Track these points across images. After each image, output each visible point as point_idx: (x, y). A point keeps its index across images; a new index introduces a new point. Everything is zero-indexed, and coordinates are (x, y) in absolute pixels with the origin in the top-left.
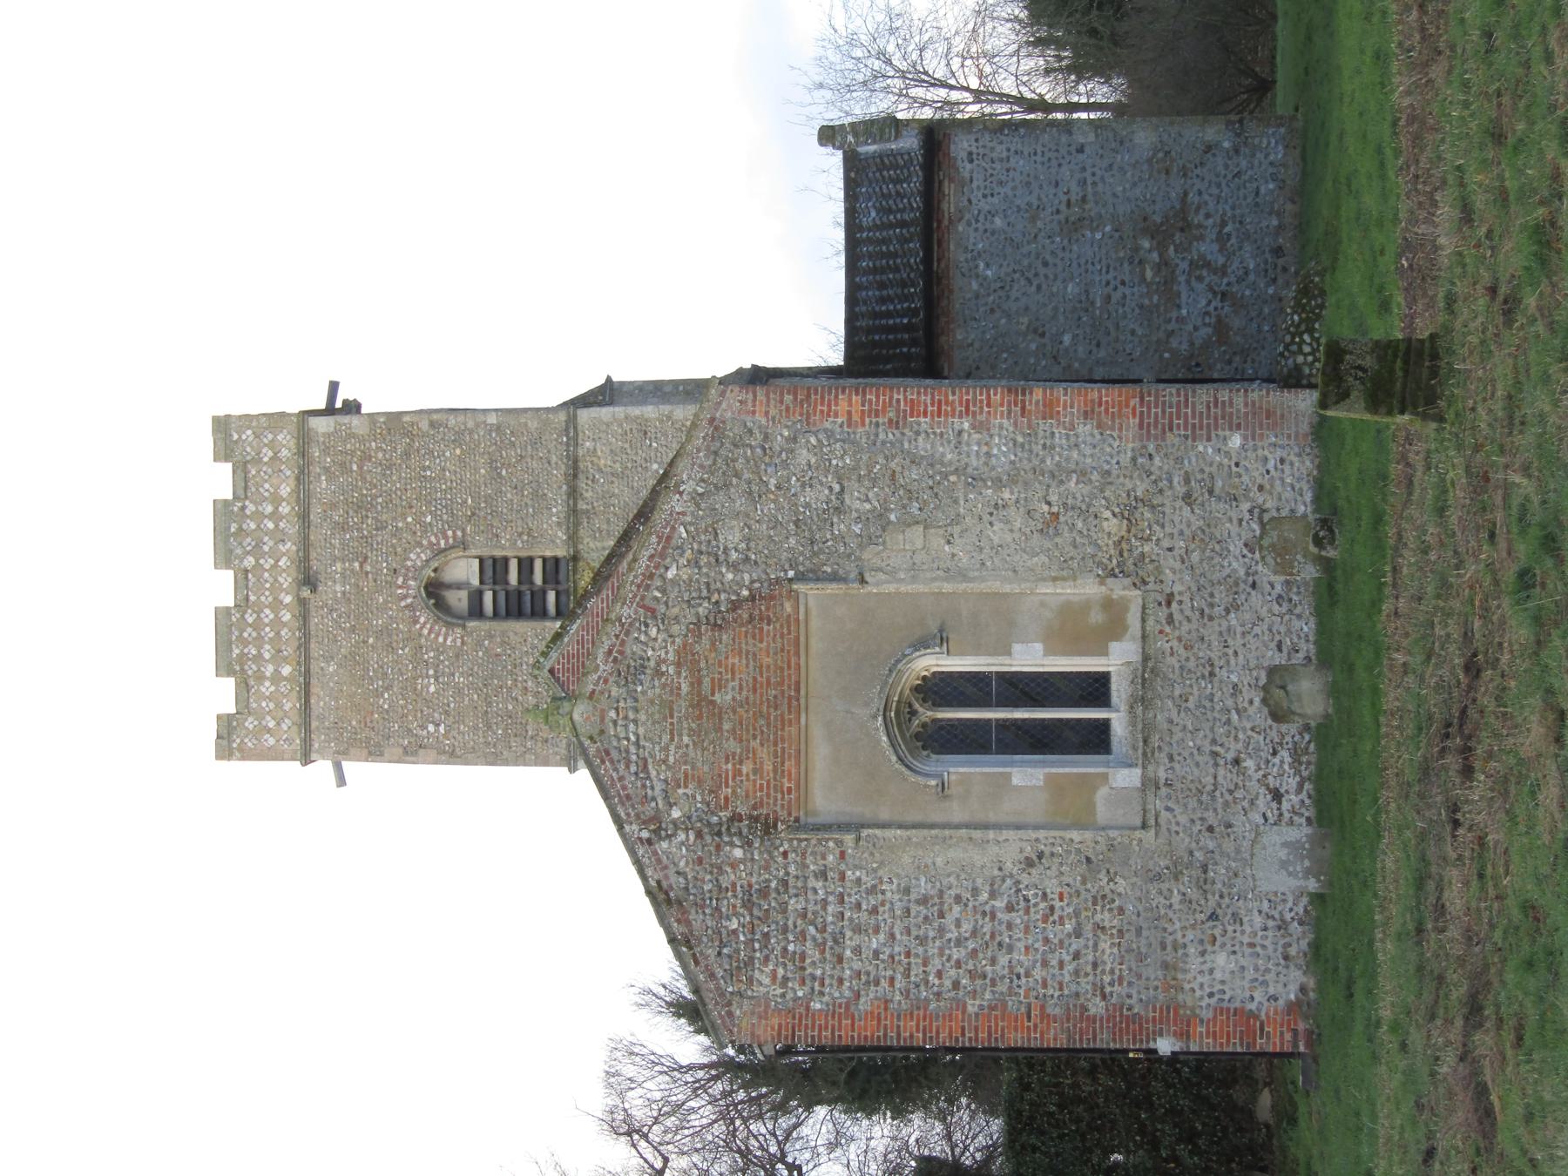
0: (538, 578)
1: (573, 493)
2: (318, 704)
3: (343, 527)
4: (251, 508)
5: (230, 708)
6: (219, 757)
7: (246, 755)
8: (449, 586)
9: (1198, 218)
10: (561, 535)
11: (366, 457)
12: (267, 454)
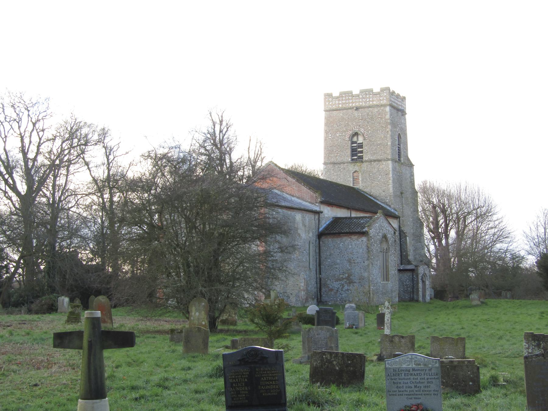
0: (359, 155)
1: (375, 161)
2: (335, 113)
3: (368, 115)
4: (371, 96)
7: (325, 98)
9: (351, 286)
10: (367, 159)
11: (381, 118)
12: (381, 98)
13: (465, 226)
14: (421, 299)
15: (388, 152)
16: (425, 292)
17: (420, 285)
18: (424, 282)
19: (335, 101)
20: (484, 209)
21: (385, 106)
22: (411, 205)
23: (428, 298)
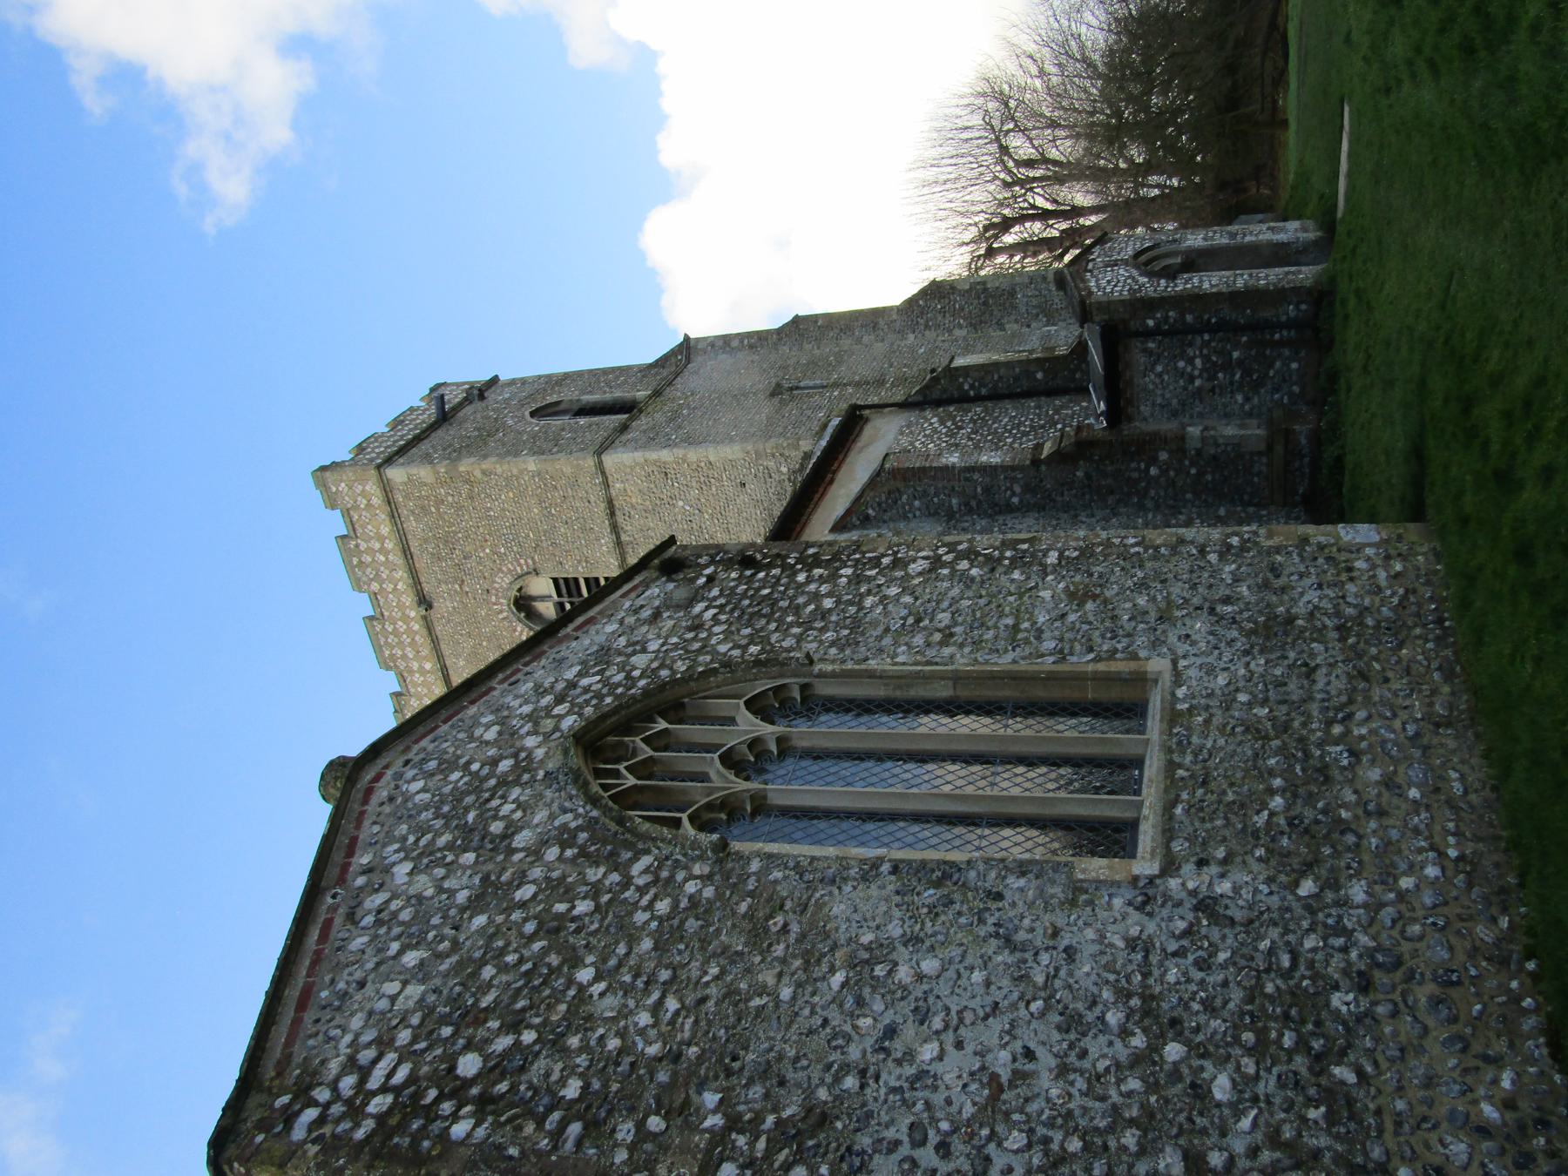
4: (363, 546)
8: (534, 599)
11: (440, 502)
13: (1046, 161)
14: (1305, 274)
15: (568, 470)
16: (1254, 248)
17: (1209, 281)
18: (1194, 262)
19: (416, 685)
20: (992, 105)
21: (387, 489)
22: (846, 342)
23: (1291, 231)
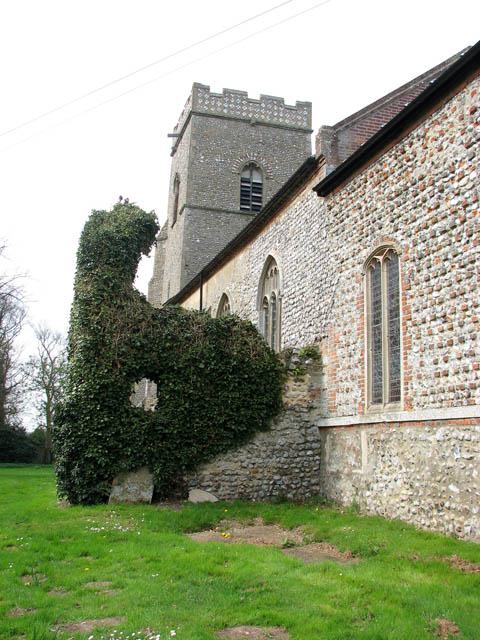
2: (212, 120)
5: (212, 91)
6: (195, 84)
